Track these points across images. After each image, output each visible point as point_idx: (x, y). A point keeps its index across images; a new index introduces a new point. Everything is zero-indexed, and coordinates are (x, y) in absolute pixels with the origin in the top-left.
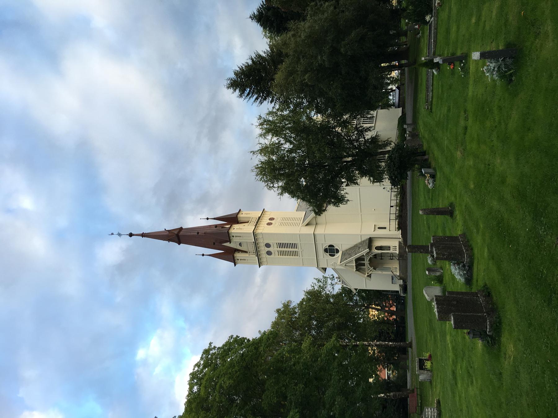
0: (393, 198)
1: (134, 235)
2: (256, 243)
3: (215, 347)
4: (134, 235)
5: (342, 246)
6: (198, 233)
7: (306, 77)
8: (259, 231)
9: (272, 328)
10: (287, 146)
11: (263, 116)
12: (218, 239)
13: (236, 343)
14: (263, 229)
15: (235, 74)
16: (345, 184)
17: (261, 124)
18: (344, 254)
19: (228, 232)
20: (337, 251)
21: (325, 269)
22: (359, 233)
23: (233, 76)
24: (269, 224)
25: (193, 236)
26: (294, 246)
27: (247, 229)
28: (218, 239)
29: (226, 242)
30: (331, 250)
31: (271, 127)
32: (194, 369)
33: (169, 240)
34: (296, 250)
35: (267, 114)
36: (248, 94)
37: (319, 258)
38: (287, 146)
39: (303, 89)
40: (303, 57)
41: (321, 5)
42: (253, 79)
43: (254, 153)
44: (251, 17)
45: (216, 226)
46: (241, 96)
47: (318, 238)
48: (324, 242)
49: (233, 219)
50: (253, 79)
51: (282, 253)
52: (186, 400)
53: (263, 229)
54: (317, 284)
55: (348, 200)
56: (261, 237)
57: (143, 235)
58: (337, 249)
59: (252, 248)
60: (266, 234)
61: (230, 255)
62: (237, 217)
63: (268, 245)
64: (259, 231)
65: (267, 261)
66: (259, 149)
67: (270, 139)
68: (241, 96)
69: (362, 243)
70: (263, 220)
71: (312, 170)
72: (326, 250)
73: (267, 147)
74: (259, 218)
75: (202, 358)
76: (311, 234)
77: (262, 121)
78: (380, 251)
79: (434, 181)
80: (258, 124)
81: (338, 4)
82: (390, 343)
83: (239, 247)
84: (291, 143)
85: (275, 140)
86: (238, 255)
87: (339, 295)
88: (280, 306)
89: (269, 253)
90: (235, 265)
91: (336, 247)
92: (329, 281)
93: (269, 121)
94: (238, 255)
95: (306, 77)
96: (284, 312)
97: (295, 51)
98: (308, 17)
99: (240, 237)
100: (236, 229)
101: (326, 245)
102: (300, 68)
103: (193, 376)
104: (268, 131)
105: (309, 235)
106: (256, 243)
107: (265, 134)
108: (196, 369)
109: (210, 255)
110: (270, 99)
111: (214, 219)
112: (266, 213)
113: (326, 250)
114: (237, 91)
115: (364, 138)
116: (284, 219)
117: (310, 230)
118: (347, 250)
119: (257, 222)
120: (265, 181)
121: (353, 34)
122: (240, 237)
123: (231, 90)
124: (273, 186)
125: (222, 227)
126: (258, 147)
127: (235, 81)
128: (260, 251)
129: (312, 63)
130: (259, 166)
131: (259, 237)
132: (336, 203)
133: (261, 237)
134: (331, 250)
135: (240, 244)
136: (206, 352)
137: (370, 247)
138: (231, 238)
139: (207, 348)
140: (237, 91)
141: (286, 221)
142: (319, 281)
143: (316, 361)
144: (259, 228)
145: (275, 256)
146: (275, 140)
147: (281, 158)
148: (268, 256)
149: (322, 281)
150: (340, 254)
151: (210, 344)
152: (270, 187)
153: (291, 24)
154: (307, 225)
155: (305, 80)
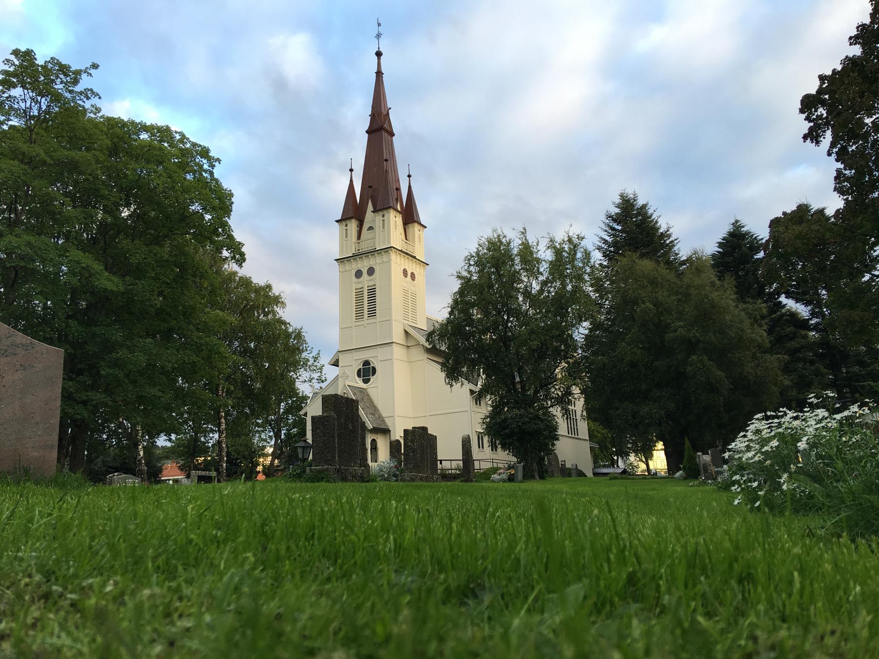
0: (454, 464)
1: (379, 59)
2: (373, 252)
3: (213, 166)
4: (379, 59)
5: (375, 388)
6: (386, 160)
7: (649, 305)
8: (394, 257)
9: (241, 278)
10: (536, 287)
11: (583, 243)
12: (379, 192)
13: (222, 202)
14: (398, 263)
15: (644, 206)
16: (473, 387)
17: (570, 240)
18: (362, 390)
19: (390, 207)
20: (366, 381)
21: (336, 364)
22: (396, 414)
23: (640, 202)
24: (405, 272)
25: (381, 153)
26: (372, 313)
27: (396, 237)
28: (379, 192)
29: (374, 206)
30: (367, 371)
31: (565, 258)
32: (176, 132)
33: (373, 116)
34: (366, 316)
35: (586, 250)
36: (613, 229)
37: (354, 353)
38: (536, 287)
39: (625, 305)
40: (679, 300)
41: (761, 326)
42: (634, 230)
43: (523, 233)
44: (737, 221)
45: (398, 189)
46: (609, 216)
47: (386, 349)
48: (380, 358)
49: (410, 216)
50: (634, 230)
51: (359, 294)
52: (126, 120)
53: (398, 263)
54: (311, 355)
55: (452, 386)
56: (384, 260)
57: (379, 74)
58: (369, 380)
59: (365, 246)
60: (390, 267)
61: (353, 212)
62: (415, 222)
63: (371, 271)
64: (394, 257)
65: (346, 271)
66: (530, 242)
67: (546, 255)
68: (609, 216)
69: (381, 419)
70: (410, 263)
71: (496, 328)
72: (366, 363)
73: (532, 253)
74: (415, 257)
75: (194, 145)
76: (392, 338)
77: (575, 241)
78: (369, 446)
79: (504, 481)
80: (571, 234)
81: (765, 352)
82: (225, 465)
83: (366, 226)
84: (541, 291)
85: (544, 267)
86: (353, 225)
87: (293, 392)
88: (276, 291)
89: (359, 274)
90: (337, 221)
91: (372, 379)
92: (316, 375)
93: (575, 254)
94: (353, 225)
95: (648, 304)
96: (267, 296)
97: (689, 287)
98: (742, 306)
99: (383, 227)
100: (395, 219)
101: (375, 363)
102: (662, 295)
103: (165, 133)
104: (558, 252)
105: (391, 336)
106: (373, 252)
107: (555, 247)
108: (178, 137)
109: (351, 181)
110: (605, 263)
111: (410, 187)
112: (422, 269)
113: (366, 363)
114: (618, 210)
115: (552, 406)
116: (414, 295)
117: (398, 336)
118: (368, 395)
119: (407, 254)
120: (478, 254)
121: (719, 373)
122: (383, 227)
123: (618, 200)
124: (470, 265)
125: (397, 199)
126: (532, 240)
127: (633, 205)
128: (361, 260)
129: (671, 314)
130: (504, 240)
131: (385, 257)
132: (448, 367)
133: (384, 260)
134: (367, 371)
135: (371, 228)
136: (205, 153)
137: (375, 430)
138: (381, 213)
139: (212, 154)
140: (618, 210)
141: (410, 299)
142: (315, 359)
143: (198, 330)
144: (398, 257)
145: (355, 284)
146: (544, 267)
147: (515, 277)
148: (354, 272)
149: (316, 364)
150: (361, 385)
151: (219, 160)
152: (469, 260)
153: (730, 281)
154: (406, 332)
155: (644, 302)
